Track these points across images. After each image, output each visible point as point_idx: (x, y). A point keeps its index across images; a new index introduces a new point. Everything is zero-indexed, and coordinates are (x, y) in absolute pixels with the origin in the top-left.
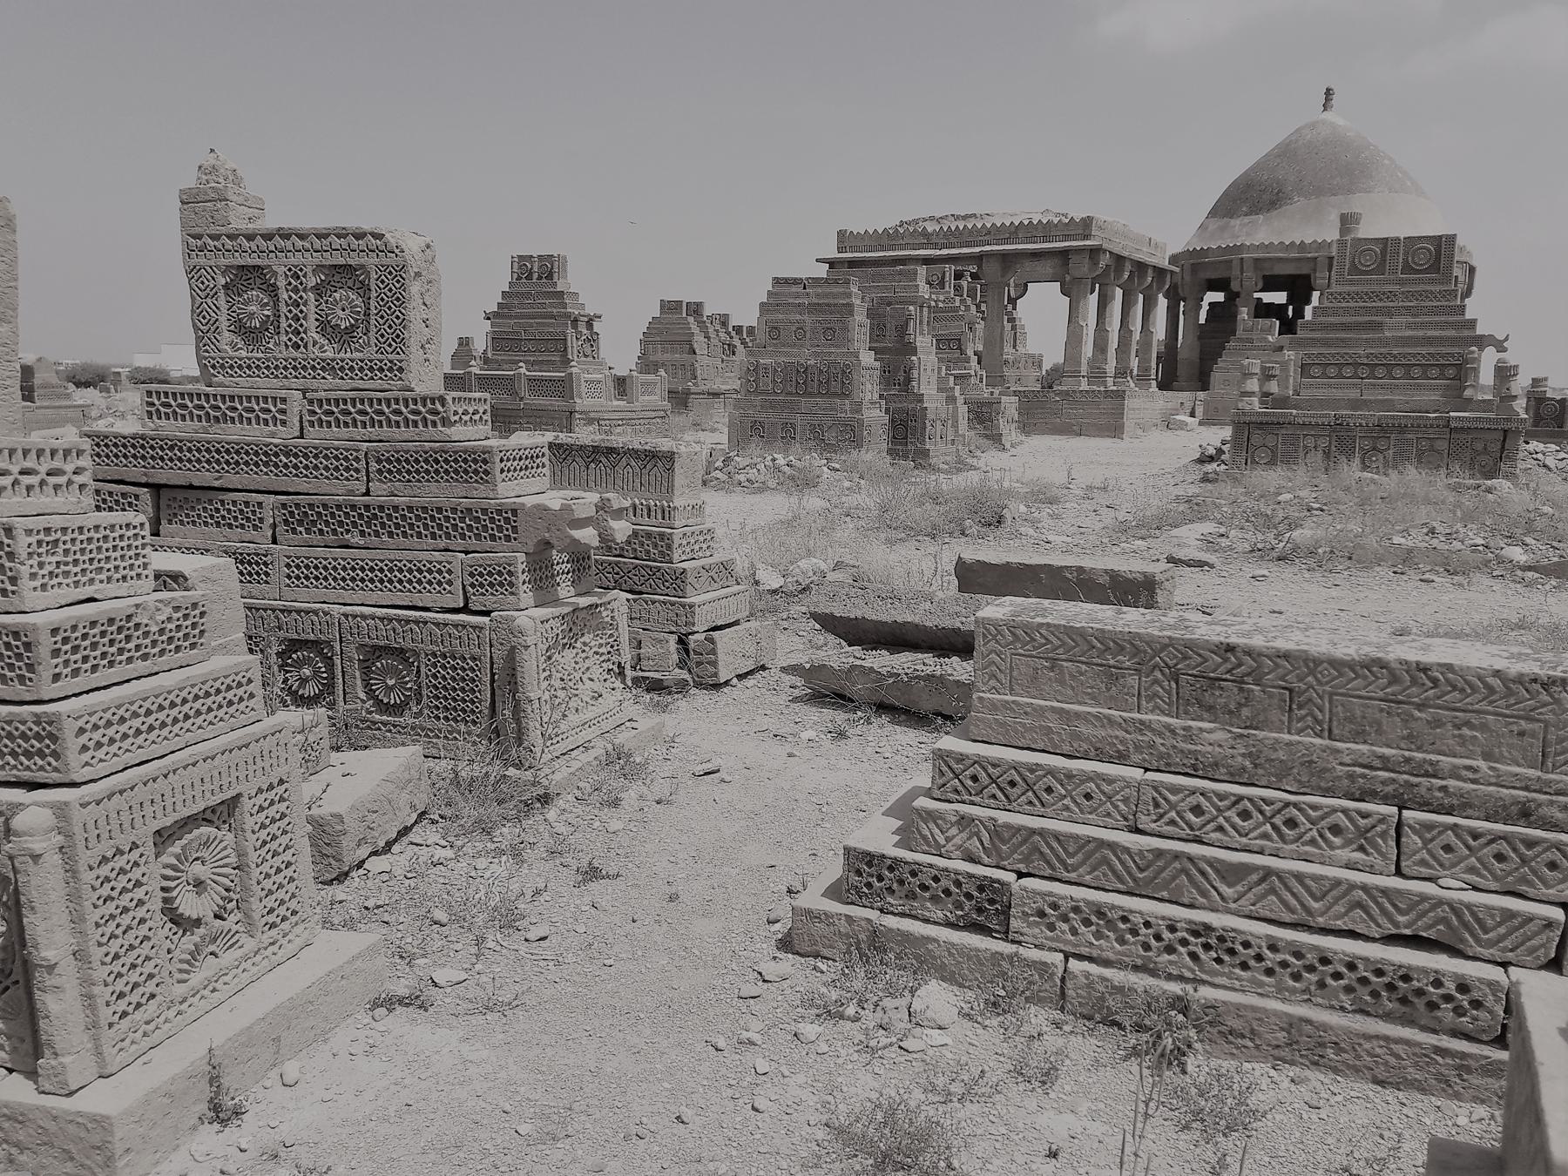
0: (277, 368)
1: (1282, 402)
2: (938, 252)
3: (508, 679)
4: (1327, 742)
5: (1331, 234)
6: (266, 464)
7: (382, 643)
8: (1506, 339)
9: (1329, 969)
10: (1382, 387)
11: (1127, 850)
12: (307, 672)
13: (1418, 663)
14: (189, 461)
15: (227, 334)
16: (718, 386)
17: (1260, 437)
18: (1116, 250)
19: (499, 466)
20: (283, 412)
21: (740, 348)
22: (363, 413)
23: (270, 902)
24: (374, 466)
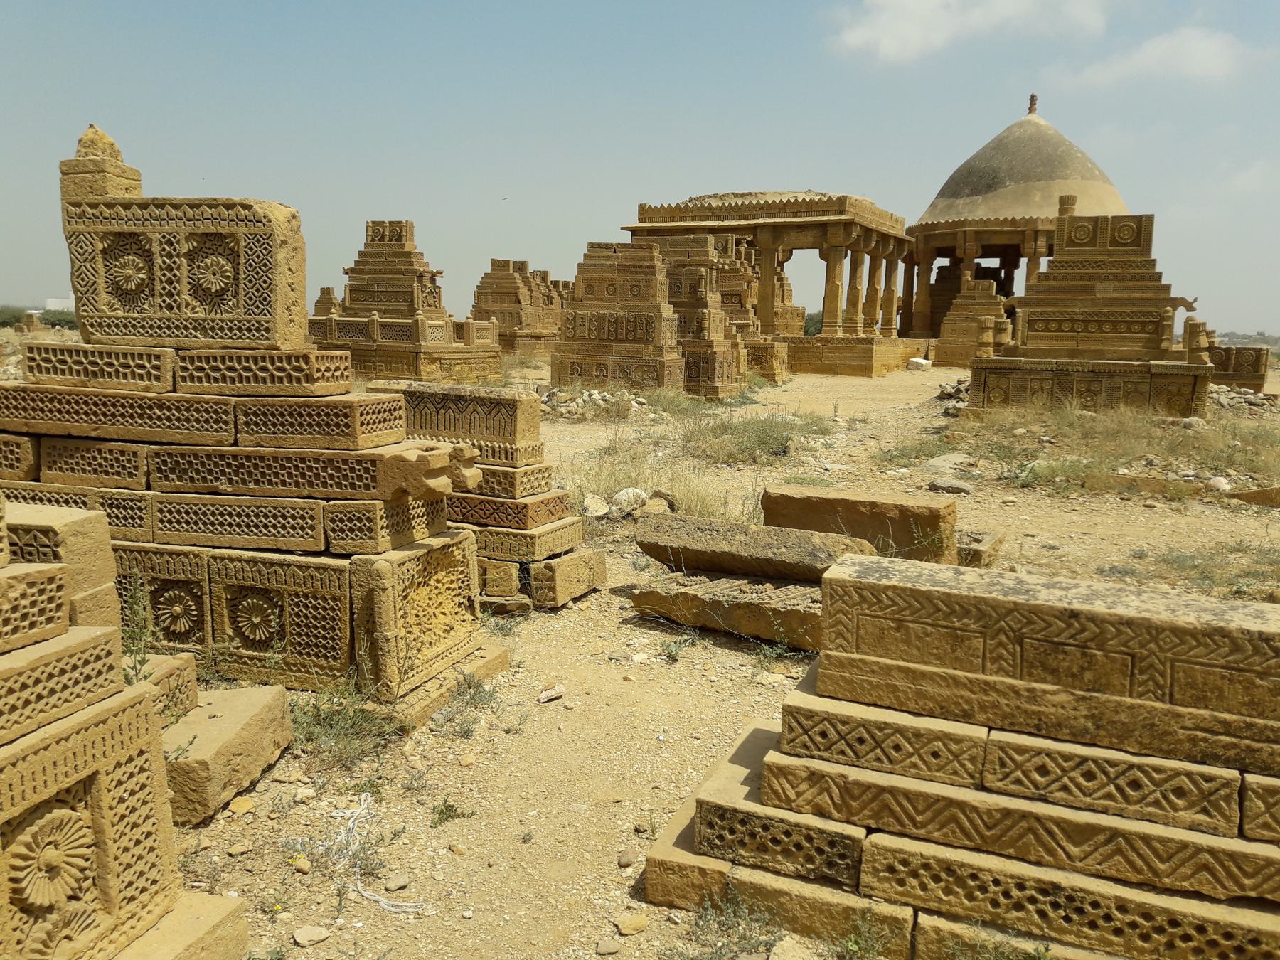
0: (151, 327)
1: (1012, 351)
2: (721, 224)
3: (366, 618)
4: (1168, 706)
5: (1052, 212)
6: (141, 416)
7: (248, 584)
8: (1195, 300)
9: (1179, 931)
10: (1095, 339)
11: (975, 809)
12: (178, 609)
13: (1260, 633)
14: (68, 412)
15: (104, 296)
16: (538, 330)
17: (994, 382)
18: (865, 223)
19: (358, 420)
20: (157, 368)
21: (557, 299)
22: (232, 369)
23: (128, 876)
24: (242, 419)
